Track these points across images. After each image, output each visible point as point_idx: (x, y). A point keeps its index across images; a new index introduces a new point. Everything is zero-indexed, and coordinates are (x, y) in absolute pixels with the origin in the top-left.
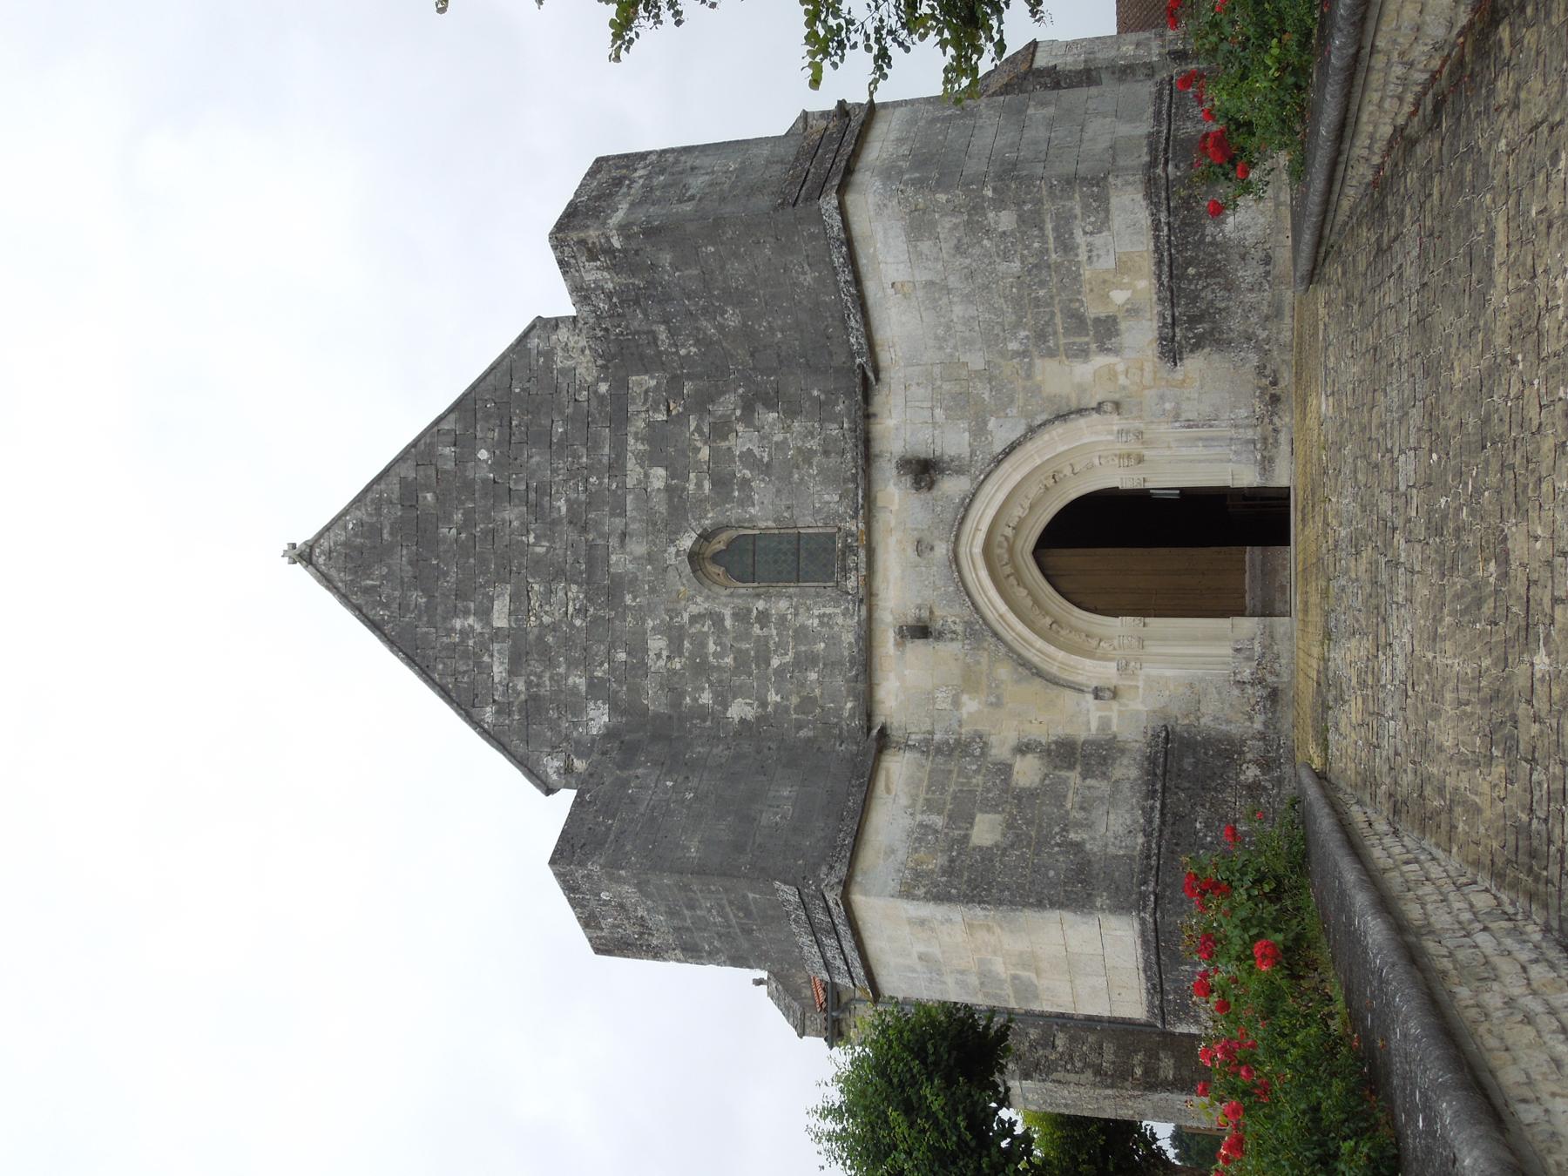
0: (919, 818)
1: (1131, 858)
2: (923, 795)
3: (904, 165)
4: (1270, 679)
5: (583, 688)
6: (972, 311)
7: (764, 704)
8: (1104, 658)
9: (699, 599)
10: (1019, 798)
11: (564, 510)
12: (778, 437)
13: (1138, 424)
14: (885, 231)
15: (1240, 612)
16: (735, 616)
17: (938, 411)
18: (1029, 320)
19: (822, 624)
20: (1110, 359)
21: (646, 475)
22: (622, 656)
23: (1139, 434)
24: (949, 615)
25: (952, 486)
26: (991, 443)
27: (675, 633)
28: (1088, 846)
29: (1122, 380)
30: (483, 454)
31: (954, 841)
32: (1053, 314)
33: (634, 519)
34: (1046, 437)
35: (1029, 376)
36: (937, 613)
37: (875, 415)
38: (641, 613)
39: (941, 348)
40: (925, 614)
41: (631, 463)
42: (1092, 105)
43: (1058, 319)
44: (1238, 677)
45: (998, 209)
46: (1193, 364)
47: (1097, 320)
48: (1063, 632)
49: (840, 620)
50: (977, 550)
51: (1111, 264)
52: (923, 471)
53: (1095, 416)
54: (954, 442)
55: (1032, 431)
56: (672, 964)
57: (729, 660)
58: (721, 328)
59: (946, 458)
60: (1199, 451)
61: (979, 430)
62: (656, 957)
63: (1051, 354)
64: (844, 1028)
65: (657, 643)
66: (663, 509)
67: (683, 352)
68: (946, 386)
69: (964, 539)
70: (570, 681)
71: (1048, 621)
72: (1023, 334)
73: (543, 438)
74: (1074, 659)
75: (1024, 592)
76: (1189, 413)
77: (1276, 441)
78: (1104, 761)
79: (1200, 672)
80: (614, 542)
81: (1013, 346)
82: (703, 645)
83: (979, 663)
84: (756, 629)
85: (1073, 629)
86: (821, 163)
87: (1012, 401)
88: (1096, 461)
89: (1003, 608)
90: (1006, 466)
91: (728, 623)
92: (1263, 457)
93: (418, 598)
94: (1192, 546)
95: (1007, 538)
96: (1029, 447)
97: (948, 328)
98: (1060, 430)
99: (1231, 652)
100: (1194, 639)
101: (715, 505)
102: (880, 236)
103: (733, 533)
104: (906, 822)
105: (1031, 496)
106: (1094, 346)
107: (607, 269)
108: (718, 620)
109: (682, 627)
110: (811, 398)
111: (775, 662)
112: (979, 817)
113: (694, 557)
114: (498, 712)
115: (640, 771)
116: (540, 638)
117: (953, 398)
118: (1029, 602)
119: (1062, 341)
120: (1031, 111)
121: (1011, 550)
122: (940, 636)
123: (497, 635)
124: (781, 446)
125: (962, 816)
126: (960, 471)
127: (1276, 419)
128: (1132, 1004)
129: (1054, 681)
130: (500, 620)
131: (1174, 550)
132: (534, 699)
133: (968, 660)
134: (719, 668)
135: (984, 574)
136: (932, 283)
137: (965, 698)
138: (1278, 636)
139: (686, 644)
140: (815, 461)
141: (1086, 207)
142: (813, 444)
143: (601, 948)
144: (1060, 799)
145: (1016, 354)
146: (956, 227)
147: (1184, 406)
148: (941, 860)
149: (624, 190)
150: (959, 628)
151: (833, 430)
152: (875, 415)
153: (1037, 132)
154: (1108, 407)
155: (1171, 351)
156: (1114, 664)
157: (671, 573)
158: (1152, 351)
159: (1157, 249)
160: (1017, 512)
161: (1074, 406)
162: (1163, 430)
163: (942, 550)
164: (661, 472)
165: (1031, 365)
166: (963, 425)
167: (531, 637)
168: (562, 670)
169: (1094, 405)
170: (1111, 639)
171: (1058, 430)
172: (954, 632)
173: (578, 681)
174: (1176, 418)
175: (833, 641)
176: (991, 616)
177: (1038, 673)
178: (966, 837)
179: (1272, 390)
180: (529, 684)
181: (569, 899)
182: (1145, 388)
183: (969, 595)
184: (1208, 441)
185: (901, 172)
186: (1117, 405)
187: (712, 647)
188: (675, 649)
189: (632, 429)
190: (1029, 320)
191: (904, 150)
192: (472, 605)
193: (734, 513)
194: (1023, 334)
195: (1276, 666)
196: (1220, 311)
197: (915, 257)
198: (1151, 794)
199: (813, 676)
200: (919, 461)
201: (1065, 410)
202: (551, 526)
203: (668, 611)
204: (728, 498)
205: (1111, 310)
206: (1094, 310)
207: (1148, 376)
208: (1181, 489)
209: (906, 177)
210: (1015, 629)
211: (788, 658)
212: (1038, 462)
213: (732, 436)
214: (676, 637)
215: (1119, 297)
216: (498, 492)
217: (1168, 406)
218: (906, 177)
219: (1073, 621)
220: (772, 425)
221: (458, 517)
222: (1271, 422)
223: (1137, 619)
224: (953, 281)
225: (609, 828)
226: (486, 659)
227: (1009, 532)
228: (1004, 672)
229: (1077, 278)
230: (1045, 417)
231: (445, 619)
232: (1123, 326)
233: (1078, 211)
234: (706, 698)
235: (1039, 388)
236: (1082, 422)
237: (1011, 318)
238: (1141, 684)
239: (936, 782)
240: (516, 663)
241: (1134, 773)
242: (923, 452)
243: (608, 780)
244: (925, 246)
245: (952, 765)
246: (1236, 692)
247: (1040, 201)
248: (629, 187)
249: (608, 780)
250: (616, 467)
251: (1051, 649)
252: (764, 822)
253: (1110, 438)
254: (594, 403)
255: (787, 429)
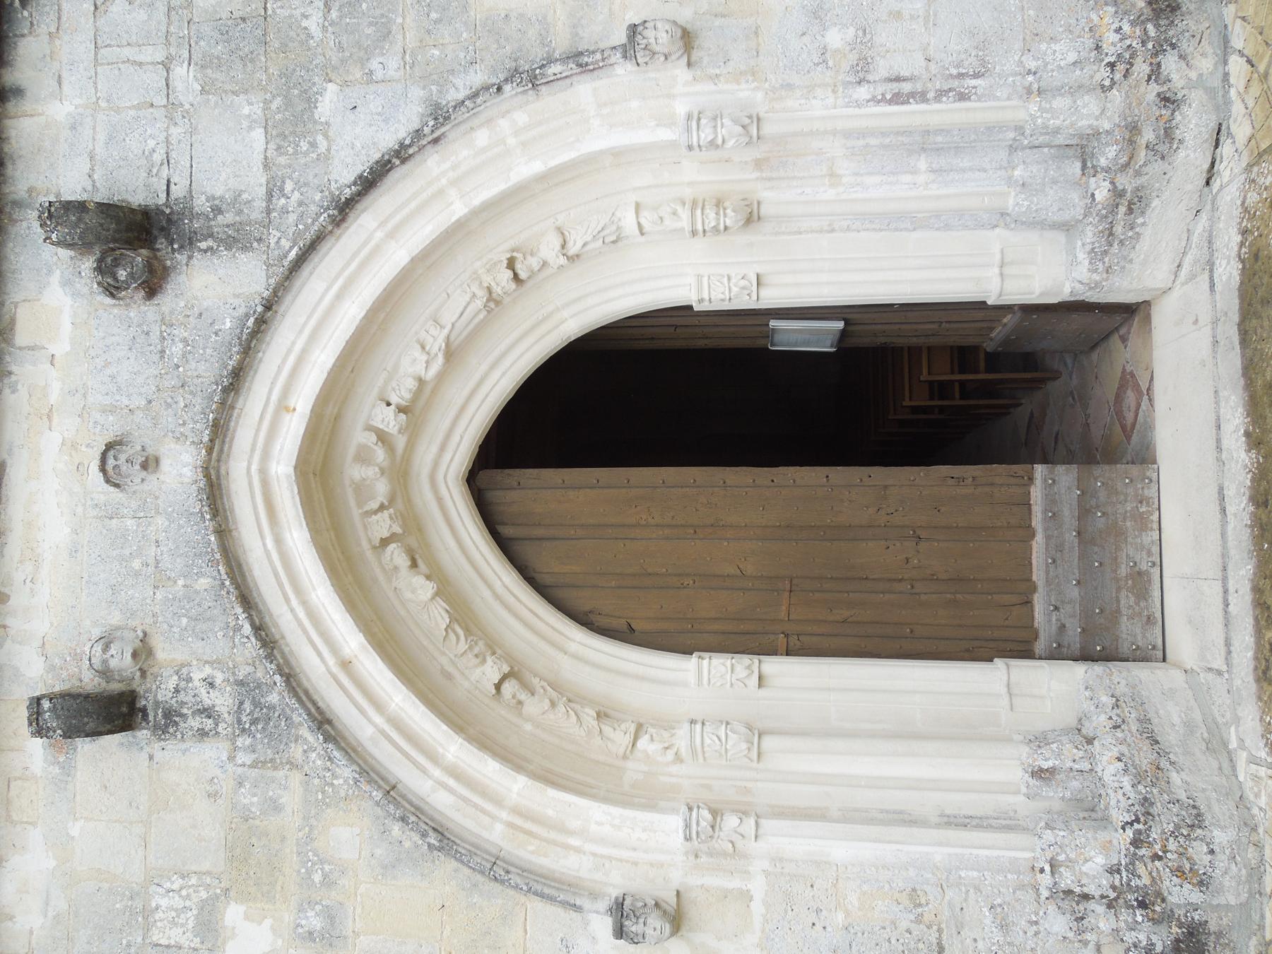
4: (1180, 895)
8: (644, 797)
13: (748, 94)
15: (1019, 646)
17: (180, 71)
23: (752, 125)
24: (197, 659)
25: (212, 286)
26: (326, 158)
34: (482, 137)
36: (165, 652)
37: (18, 92)
40: (121, 660)
44: (1067, 880)
48: (533, 706)
50: (283, 467)
52: (133, 241)
53: (623, 70)
54: (218, 157)
59: (201, 204)
60: (916, 186)
69: (244, 435)
71: (491, 671)
74: (552, 801)
75: (422, 589)
77: (1168, 133)
79: (939, 854)
83: (275, 807)
85: (566, 695)
87: (385, 35)
88: (628, 221)
89: (352, 641)
90: (366, 222)
92: (1118, 193)
94: (801, 465)
95: (382, 437)
96: (433, 166)
98: (521, 118)
99: (1017, 775)
100: (905, 734)
105: (448, 318)
117: (224, 34)
118: (438, 616)
121: (400, 473)
122: (170, 720)
126: (237, 240)
127: (1170, 63)
129: (496, 869)
131: (763, 475)
133: (247, 798)
135: (298, 538)
137: (233, 914)
138: (1170, 738)
150: (223, 701)
152: (18, 92)
154: (660, 38)
156: (672, 824)
160: (408, 362)
162: (824, 109)
163: (181, 466)
166: (250, 107)
170: (668, 725)
171: (516, 115)
172: (207, 712)
174: (861, 72)
176: (315, 667)
177: (443, 839)
183: (247, 600)
186: (687, 39)
195: (1198, 851)
200: (108, 210)
208: (850, 314)
210: (378, 702)
212: (459, 209)
217: (835, 38)
219: (569, 670)
222: (1155, 73)
223: (746, 659)
227: (388, 420)
228: (350, 834)
230: (478, 77)
236: (584, 91)
238: (757, 886)
242: (138, 191)
246: (1058, 923)
251: (489, 769)
253: (665, 135)
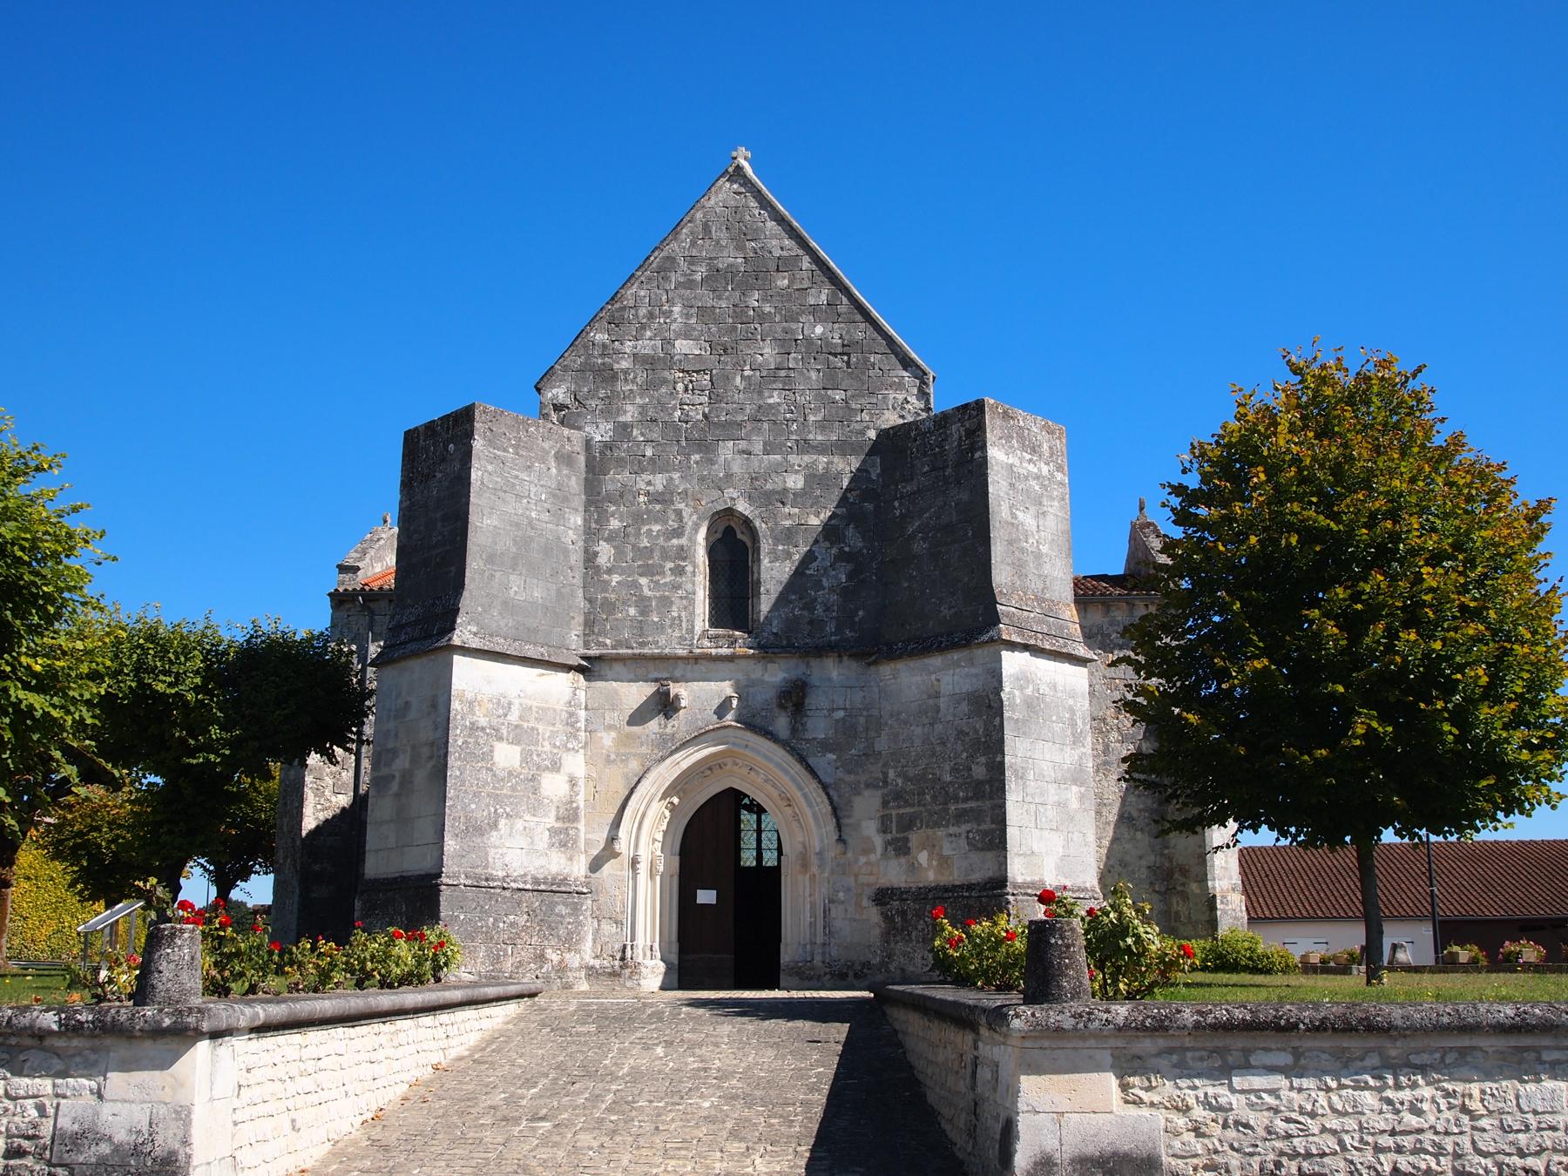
0: (516, 702)
1: (486, 867)
2: (535, 704)
3: (1029, 691)
5: (622, 419)
6: (918, 742)
7: (610, 571)
9: (695, 517)
10: (534, 778)
11: (771, 401)
12: (825, 583)
14: (976, 675)
16: (681, 548)
18: (910, 787)
19: (674, 619)
20: (879, 850)
21: (797, 472)
22: (649, 453)
27: (667, 497)
28: (494, 833)
29: (863, 860)
30: (819, 330)
31: (497, 730)
32: (913, 805)
33: (761, 461)
35: (868, 786)
38: (684, 468)
39: (892, 716)
41: (807, 458)
42: (1076, 836)
43: (908, 810)
45: (987, 765)
46: (873, 914)
47: (907, 840)
49: (677, 634)
51: (946, 852)
54: (818, 727)
55: (825, 787)
56: (398, 497)
57: (645, 543)
58: (912, 537)
61: (825, 746)
62: (403, 483)
63: (885, 804)
64: (348, 606)
65: (659, 481)
66: (769, 486)
67: (896, 504)
68: (862, 720)
70: (629, 408)
72: (900, 781)
73: (830, 383)
76: (836, 911)
78: (563, 845)
80: (743, 445)
81: (891, 774)
82: (656, 522)
84: (670, 565)
86: (1039, 622)
91: (675, 541)
93: (701, 272)
97: (906, 723)
101: (772, 530)
102: (973, 671)
103: (749, 544)
104: (512, 693)
106: (889, 837)
107: (960, 445)
108: (678, 533)
109: (672, 502)
110: (857, 610)
111: (643, 581)
112: (518, 749)
113: (730, 512)
114: (604, 346)
115: (554, 471)
116: (665, 381)
119: (894, 813)
120: (1075, 788)
123: (668, 342)
124: (818, 585)
125: (519, 735)
126: (794, 731)
128: (374, 866)
130: (682, 346)
132: (614, 377)
134: (638, 534)
136: (938, 711)
137: (613, 734)
139: (658, 507)
140: (806, 613)
141: (985, 833)
142: (819, 610)
143: (411, 437)
144: (534, 811)
145: (885, 775)
146: (976, 731)
147: (841, 907)
148: (483, 722)
149: (1028, 457)
151: (830, 627)
153: (1053, 794)
155: (883, 896)
157: (716, 493)
158: (884, 882)
159: (955, 887)
161: (844, 821)
164: (800, 484)
165: (876, 787)
167: (666, 374)
168: (638, 400)
169: (844, 837)
173: (630, 414)
175: (660, 628)
178: (500, 739)
179: (851, 973)
180: (626, 372)
181: (448, 416)
182: (856, 876)
184: (813, 925)
185: (1022, 689)
187: (656, 528)
188: (655, 498)
189: (836, 459)
190: (910, 787)
191: (1044, 689)
192: (693, 321)
193: (765, 546)
194: (900, 781)
196: (909, 934)
197: (957, 699)
198: (536, 881)
199: (632, 611)
201: (840, 814)
202: (757, 388)
203: (686, 491)
204: (777, 541)
205: (914, 851)
206: (914, 838)
207: (863, 879)
209: (1017, 693)
211: (647, 592)
213: (827, 544)
214: (662, 498)
215: (923, 857)
216: (786, 345)
217: (841, 894)
218: (1017, 693)
220: (836, 577)
221: (767, 309)
224: (939, 727)
225: (505, 450)
226: (648, 333)
229: (937, 825)
231: (681, 297)
232: (903, 860)
233: (983, 827)
234: (615, 524)
235: (859, 794)
237: (911, 772)
239: (544, 713)
240: (647, 362)
241: (554, 869)
243: (546, 445)
244: (964, 707)
245: (559, 727)
247: (991, 798)
248: (1030, 461)
249: (546, 445)
250: (804, 446)
252: (512, 578)
254: (858, 427)
255: (832, 590)
